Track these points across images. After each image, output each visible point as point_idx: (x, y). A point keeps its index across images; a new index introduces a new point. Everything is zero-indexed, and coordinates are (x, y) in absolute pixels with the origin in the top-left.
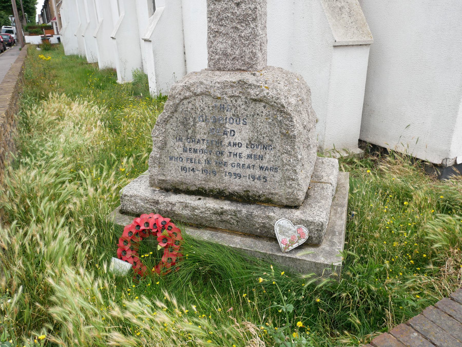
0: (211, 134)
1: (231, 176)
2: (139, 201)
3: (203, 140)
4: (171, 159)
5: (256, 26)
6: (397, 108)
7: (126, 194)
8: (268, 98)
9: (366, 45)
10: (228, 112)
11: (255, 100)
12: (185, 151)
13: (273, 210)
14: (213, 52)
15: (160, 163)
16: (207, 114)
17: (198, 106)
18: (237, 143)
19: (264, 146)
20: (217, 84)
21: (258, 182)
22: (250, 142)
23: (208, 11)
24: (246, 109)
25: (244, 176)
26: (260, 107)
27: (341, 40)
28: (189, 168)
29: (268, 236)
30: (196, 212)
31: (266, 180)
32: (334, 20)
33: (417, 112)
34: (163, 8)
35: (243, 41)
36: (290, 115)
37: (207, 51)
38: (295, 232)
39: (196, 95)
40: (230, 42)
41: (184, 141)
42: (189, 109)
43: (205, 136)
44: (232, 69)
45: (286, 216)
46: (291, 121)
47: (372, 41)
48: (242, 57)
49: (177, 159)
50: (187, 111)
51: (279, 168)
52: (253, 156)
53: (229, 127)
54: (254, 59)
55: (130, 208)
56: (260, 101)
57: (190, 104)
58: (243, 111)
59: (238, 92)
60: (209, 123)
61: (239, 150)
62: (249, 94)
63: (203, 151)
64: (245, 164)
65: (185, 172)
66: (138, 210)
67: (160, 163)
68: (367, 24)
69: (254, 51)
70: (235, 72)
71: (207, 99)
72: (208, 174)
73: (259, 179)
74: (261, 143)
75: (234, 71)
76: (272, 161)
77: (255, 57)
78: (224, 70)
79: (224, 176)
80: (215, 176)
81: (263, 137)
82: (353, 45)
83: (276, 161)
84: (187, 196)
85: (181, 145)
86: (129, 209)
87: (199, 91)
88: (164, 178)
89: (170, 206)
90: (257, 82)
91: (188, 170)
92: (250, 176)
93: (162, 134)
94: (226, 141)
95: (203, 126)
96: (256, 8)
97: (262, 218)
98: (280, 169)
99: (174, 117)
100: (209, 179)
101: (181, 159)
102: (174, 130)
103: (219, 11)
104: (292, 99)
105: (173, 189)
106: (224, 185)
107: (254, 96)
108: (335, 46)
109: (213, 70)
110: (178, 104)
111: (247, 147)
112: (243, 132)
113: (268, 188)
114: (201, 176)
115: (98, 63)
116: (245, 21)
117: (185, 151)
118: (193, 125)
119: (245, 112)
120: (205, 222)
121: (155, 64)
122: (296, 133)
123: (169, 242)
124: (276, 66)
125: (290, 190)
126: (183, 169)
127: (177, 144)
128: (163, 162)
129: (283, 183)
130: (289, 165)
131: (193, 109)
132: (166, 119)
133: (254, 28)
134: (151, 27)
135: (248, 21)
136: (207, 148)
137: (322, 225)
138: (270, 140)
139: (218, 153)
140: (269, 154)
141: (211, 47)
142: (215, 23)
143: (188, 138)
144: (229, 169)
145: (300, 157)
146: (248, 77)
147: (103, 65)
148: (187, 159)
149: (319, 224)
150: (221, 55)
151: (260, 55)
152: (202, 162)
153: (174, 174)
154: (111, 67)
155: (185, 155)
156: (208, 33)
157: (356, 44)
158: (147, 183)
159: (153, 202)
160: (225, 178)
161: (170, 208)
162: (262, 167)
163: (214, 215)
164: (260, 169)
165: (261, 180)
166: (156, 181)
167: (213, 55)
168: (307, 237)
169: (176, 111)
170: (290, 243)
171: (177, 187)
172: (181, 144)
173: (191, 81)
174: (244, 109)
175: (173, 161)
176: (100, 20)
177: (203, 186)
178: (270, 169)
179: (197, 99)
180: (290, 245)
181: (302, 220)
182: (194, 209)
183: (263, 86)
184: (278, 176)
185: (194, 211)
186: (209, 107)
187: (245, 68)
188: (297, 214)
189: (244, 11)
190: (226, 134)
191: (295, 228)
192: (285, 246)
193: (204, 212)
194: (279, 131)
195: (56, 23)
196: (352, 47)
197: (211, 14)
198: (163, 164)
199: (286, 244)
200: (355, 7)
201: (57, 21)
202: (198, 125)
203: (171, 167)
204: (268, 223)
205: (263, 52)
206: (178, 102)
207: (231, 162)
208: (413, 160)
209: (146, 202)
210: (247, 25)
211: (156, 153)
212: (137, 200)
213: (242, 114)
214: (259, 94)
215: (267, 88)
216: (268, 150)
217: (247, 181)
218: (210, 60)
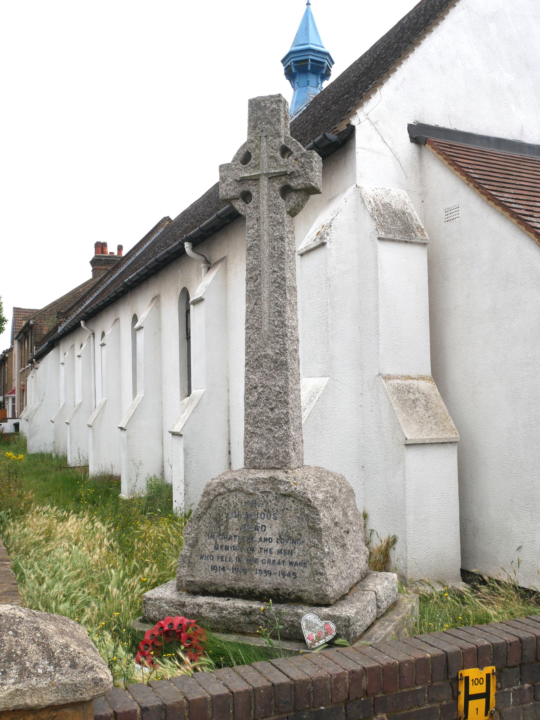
0: (243, 529)
1: (261, 573)
2: (164, 605)
3: (235, 536)
4: (202, 557)
5: (288, 428)
6: (502, 523)
7: (151, 597)
8: (296, 492)
9: (451, 443)
10: (260, 508)
11: (284, 495)
12: (216, 548)
13: (302, 607)
14: (249, 452)
15: (189, 562)
16: (239, 510)
17: (231, 502)
18: (268, 538)
19: (293, 540)
20: (250, 481)
21: (288, 579)
22: (280, 536)
23: (245, 414)
24: (276, 503)
25: (274, 573)
26: (289, 502)
27: (412, 435)
28: (220, 567)
29: (298, 638)
30: (224, 613)
31: (296, 576)
32: (405, 415)
33: (524, 527)
34: (202, 391)
35: (276, 441)
36: (316, 509)
37: (243, 450)
38: (322, 628)
39: (230, 491)
40: (265, 442)
41: (216, 537)
42: (222, 505)
43: (237, 532)
44: (267, 468)
45: (314, 612)
46: (317, 515)
47: (458, 438)
48: (276, 456)
49: (208, 558)
50: (221, 507)
51: (308, 563)
52: (283, 551)
53: (261, 522)
54: (288, 458)
55: (153, 614)
56: (289, 496)
57: (224, 500)
58: (273, 506)
59: (269, 488)
60: (242, 519)
61: (270, 546)
62: (279, 489)
63: (234, 548)
64: (275, 560)
65: (215, 572)
66: (162, 616)
67: (189, 562)
68: (450, 417)
69: (287, 450)
70: (269, 470)
71: (240, 495)
72: (239, 573)
73: (289, 575)
74: (290, 538)
75: (268, 469)
76: (301, 556)
77: (288, 456)
78: (259, 469)
79: (254, 574)
80: (245, 574)
81: (293, 532)
82: (432, 444)
83: (305, 555)
84: (216, 598)
85: (213, 542)
86: (152, 615)
87: (233, 487)
88: (192, 580)
89: (197, 608)
90: (287, 478)
91: (218, 569)
92: (280, 573)
93: (194, 530)
94: (257, 537)
95: (235, 522)
96: (288, 413)
97: (291, 616)
98: (309, 564)
99: (207, 514)
100: (240, 579)
101: (212, 558)
102: (207, 527)
103: (255, 414)
104: (320, 495)
105: (201, 592)
106: (255, 583)
107: (283, 491)
108: (407, 445)
109: (248, 469)
110: (212, 500)
111: (277, 542)
112: (274, 527)
113: (297, 584)
114: (231, 575)
115: (88, 466)
116: (279, 423)
117: (216, 548)
118: (226, 521)
119: (276, 507)
120: (233, 626)
121: (186, 466)
122: (322, 526)
123: (193, 642)
124: (313, 465)
125: (319, 586)
126: (214, 568)
127: (209, 541)
128: (193, 561)
129: (313, 578)
130: (316, 558)
131: (226, 505)
132: (199, 515)
133: (286, 430)
134: (183, 416)
135: (281, 423)
136: (238, 544)
137: (349, 620)
138: (299, 534)
139: (249, 549)
140: (298, 548)
141: (247, 447)
142: (251, 425)
143: (220, 535)
144: (260, 566)
145: (326, 550)
146: (280, 475)
147: (97, 470)
148: (218, 557)
149: (346, 618)
150: (257, 454)
151: (293, 454)
152: (233, 559)
153: (204, 575)
154: (110, 473)
155: (216, 553)
156: (245, 434)
157: (435, 441)
158: (174, 588)
159: (179, 605)
160: (256, 576)
161: (197, 610)
162: (291, 562)
163: (242, 617)
164: (290, 565)
165: (291, 576)
166: (184, 583)
167: (249, 454)
168: (334, 634)
169: (210, 507)
170: (316, 639)
171: (206, 589)
172: (213, 541)
173: (226, 478)
174: (275, 504)
175: (204, 560)
176: (100, 400)
177: (233, 585)
178: (300, 565)
179: (230, 495)
180: (317, 642)
181: (330, 616)
182: (222, 609)
183: (292, 481)
184: (307, 572)
185: (222, 612)
186: (242, 503)
187: (279, 466)
188: (326, 610)
189: (277, 415)
190: (258, 530)
191: (322, 624)
192: (311, 642)
193: (232, 612)
194: (306, 525)
195: (14, 399)
196: (431, 445)
197: (248, 417)
198: (193, 564)
199: (312, 640)
200: (433, 399)
201: (16, 395)
202: (230, 521)
203: (201, 566)
204: (297, 621)
205: (297, 451)
206: (212, 498)
207: (262, 558)
208: (515, 588)
209: (171, 605)
210: (280, 427)
211: (187, 551)
212: (161, 604)
213: (273, 509)
214: (287, 490)
215: (296, 484)
216: (297, 545)
217: (277, 579)
218: (246, 458)
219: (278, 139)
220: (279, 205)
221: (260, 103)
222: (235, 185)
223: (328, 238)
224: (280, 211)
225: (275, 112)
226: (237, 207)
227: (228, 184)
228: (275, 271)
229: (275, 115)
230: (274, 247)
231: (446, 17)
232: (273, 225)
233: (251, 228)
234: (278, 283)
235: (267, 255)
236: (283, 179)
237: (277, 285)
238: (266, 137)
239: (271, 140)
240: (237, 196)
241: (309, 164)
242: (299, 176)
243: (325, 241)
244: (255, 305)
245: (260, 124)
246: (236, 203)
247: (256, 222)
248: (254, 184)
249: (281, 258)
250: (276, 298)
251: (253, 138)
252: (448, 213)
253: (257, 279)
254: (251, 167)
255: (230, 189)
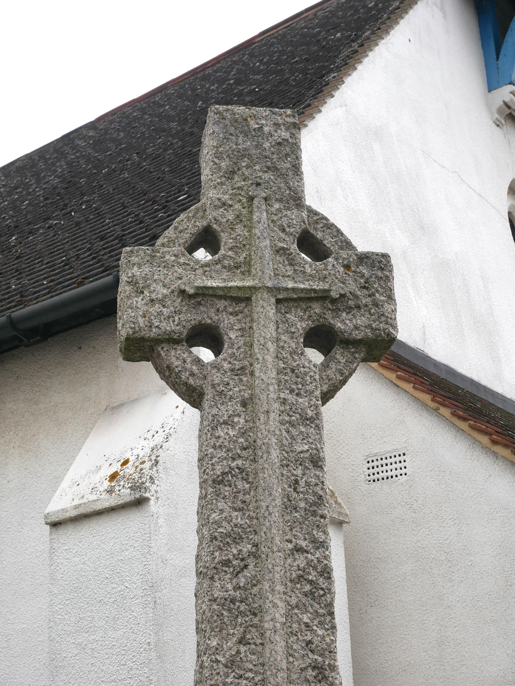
219: (295, 211)
220: (306, 374)
221: (246, 120)
222: (177, 304)
223: (153, 488)
224: (308, 388)
225: (288, 149)
226: (176, 363)
227: (152, 301)
228: (299, 549)
229: (287, 155)
230: (297, 482)
231: (323, 109)
232: (290, 422)
233: (225, 423)
234: (311, 582)
235: (278, 502)
236: (317, 308)
237: (308, 588)
238: (266, 199)
239: (277, 210)
240: (181, 333)
241: (382, 283)
242: (358, 307)
243: (147, 495)
244: (240, 642)
245: (248, 167)
246: (173, 353)
247: (239, 408)
248: (231, 310)
249: (314, 514)
250: (307, 625)
251: (227, 197)
252: (375, 464)
253: (246, 567)
254: (224, 267)
255: (160, 314)
